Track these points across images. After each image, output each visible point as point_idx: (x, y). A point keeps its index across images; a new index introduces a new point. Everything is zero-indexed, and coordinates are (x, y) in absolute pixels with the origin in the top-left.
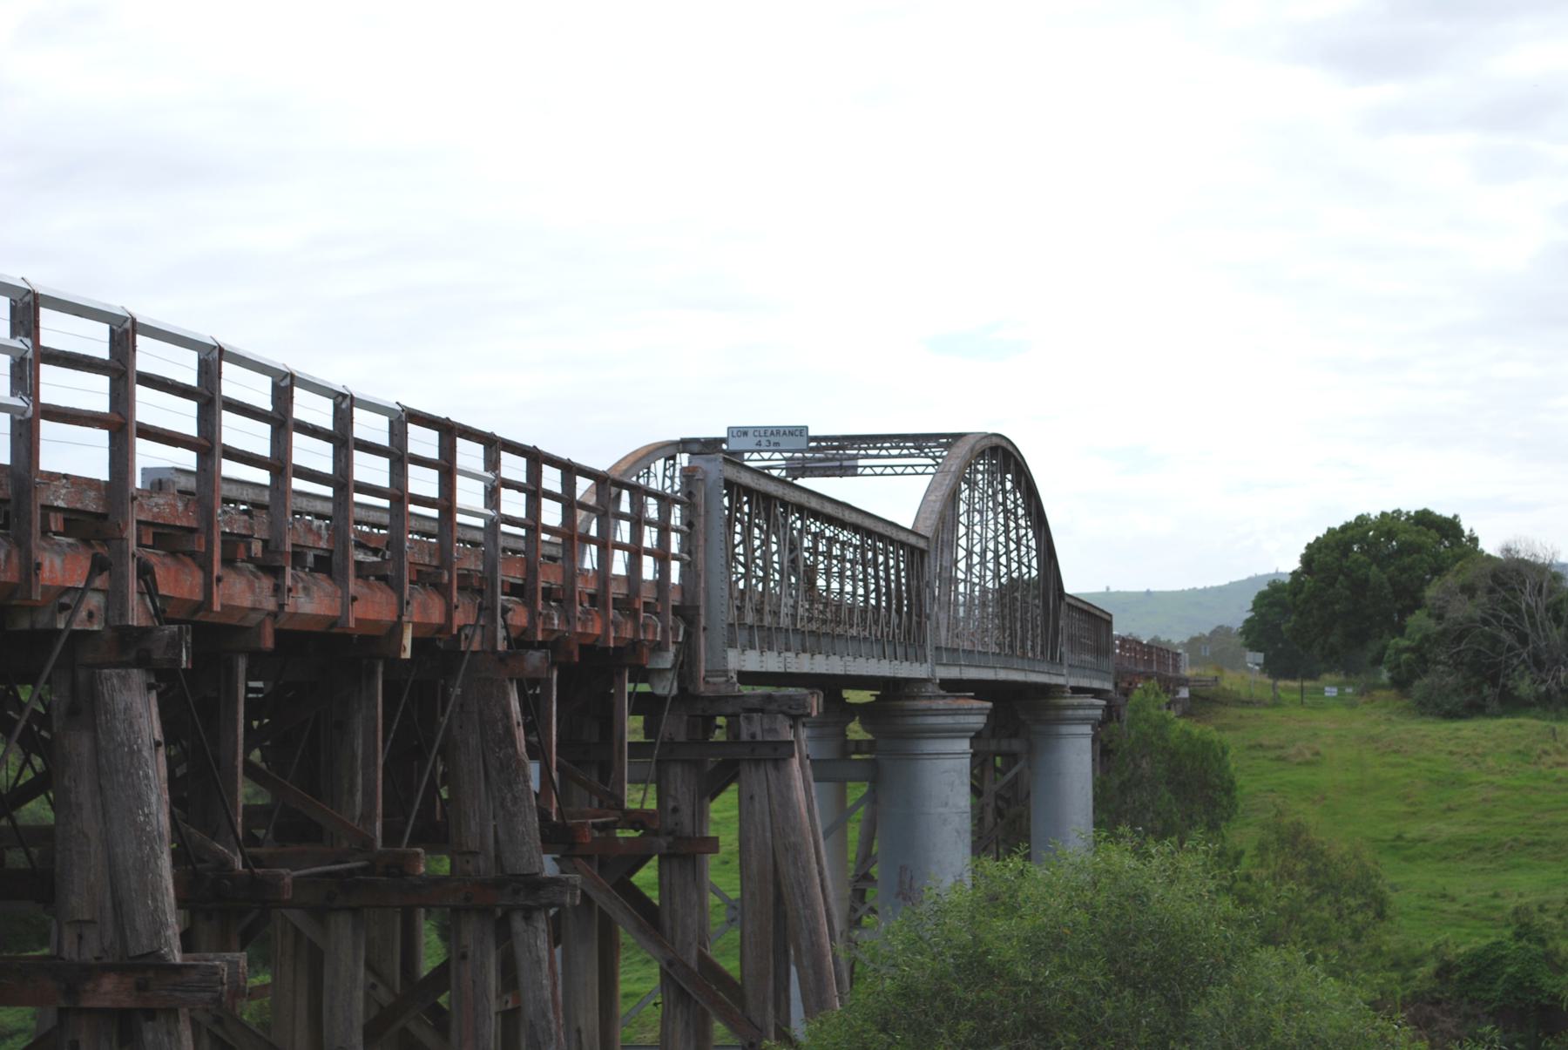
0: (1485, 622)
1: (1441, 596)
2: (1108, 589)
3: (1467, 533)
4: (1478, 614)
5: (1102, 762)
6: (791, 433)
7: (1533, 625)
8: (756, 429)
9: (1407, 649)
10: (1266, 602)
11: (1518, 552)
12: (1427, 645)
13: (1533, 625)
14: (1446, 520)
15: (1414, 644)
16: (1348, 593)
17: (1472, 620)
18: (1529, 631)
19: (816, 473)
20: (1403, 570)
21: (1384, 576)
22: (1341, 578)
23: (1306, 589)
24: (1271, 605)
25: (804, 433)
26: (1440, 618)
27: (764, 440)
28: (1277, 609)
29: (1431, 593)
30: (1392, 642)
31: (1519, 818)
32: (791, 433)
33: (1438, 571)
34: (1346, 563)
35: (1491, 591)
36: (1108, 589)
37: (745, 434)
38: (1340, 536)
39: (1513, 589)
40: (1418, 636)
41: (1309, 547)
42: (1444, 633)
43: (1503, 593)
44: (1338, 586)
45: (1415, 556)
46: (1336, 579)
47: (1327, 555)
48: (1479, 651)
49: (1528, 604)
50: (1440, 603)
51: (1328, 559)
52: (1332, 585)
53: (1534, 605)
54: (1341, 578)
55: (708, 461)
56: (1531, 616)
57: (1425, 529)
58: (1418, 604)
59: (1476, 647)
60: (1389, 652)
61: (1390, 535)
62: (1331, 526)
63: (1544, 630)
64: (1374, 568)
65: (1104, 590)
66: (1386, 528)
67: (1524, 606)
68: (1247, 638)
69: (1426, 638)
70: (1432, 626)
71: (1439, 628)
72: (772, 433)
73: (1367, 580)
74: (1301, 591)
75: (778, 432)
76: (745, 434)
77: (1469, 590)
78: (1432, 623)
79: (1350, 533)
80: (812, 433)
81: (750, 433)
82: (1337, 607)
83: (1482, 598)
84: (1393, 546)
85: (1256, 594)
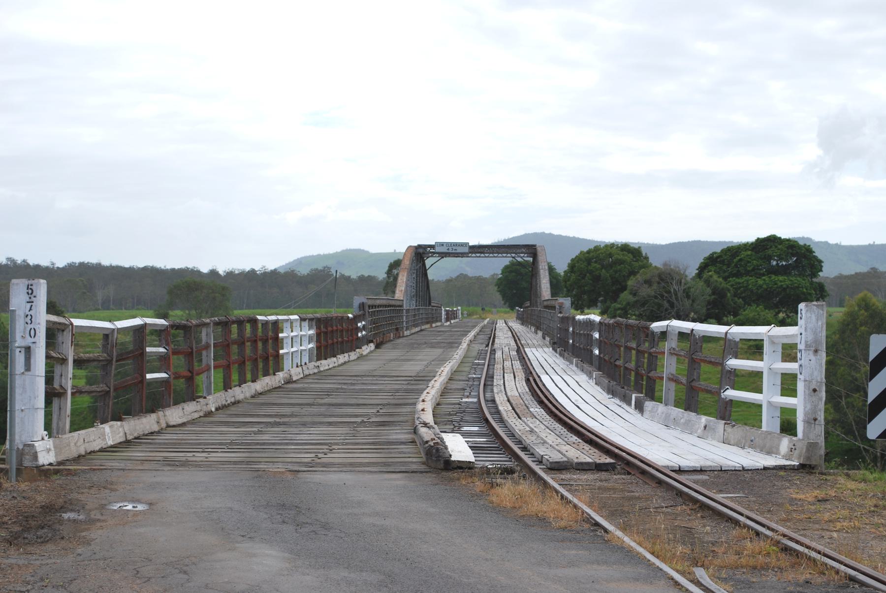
0: (656, 297)
1: (635, 285)
2: (395, 251)
3: (644, 255)
4: (653, 293)
5: (80, 312)
6: (462, 245)
7: (677, 299)
8: (447, 243)
9: (619, 309)
10: (508, 270)
11: (670, 266)
12: (628, 307)
13: (677, 299)
14: (635, 249)
15: (622, 307)
16: (591, 282)
17: (649, 296)
18: (675, 302)
19: (451, 255)
20: (616, 272)
21: (608, 275)
22: (588, 275)
23: (571, 279)
24: (511, 272)
25: (467, 245)
26: (635, 295)
27: (450, 248)
28: (514, 274)
29: (631, 283)
30: (613, 305)
31: (680, 388)
32: (462, 245)
33: (633, 273)
34: (590, 268)
35: (659, 283)
36: (395, 251)
37: (443, 245)
38: (587, 255)
39: (668, 282)
40: (624, 303)
41: (572, 260)
42: (636, 302)
43: (663, 284)
44: (586, 278)
45: (622, 265)
46: (586, 275)
47: (581, 264)
48: (652, 310)
49: (674, 289)
50: (636, 288)
51: (582, 266)
52: (583, 278)
53: (677, 290)
54: (588, 275)
55: (565, 300)
56: (676, 295)
57: (627, 253)
58: (624, 288)
59: (651, 308)
60: (610, 310)
61: (610, 255)
62: (582, 250)
63: (682, 301)
64: (603, 270)
65: (393, 251)
66: (608, 253)
67: (672, 290)
68: (498, 288)
69: (628, 304)
70: (631, 299)
71: (635, 299)
72: (454, 245)
73: (600, 276)
74: (569, 280)
75: (456, 245)
76: (443, 245)
77: (648, 282)
78: (631, 297)
79: (592, 254)
80: (470, 244)
81: (445, 245)
82: (586, 288)
83: (655, 286)
84: (609, 261)
85: (503, 266)
